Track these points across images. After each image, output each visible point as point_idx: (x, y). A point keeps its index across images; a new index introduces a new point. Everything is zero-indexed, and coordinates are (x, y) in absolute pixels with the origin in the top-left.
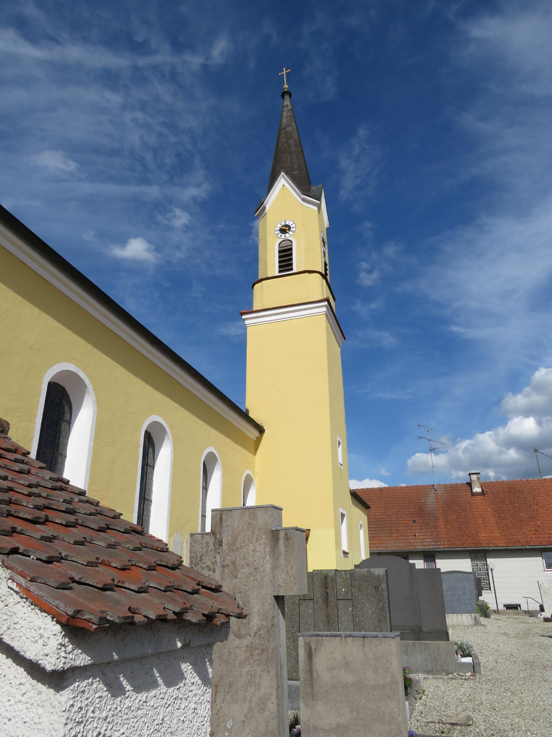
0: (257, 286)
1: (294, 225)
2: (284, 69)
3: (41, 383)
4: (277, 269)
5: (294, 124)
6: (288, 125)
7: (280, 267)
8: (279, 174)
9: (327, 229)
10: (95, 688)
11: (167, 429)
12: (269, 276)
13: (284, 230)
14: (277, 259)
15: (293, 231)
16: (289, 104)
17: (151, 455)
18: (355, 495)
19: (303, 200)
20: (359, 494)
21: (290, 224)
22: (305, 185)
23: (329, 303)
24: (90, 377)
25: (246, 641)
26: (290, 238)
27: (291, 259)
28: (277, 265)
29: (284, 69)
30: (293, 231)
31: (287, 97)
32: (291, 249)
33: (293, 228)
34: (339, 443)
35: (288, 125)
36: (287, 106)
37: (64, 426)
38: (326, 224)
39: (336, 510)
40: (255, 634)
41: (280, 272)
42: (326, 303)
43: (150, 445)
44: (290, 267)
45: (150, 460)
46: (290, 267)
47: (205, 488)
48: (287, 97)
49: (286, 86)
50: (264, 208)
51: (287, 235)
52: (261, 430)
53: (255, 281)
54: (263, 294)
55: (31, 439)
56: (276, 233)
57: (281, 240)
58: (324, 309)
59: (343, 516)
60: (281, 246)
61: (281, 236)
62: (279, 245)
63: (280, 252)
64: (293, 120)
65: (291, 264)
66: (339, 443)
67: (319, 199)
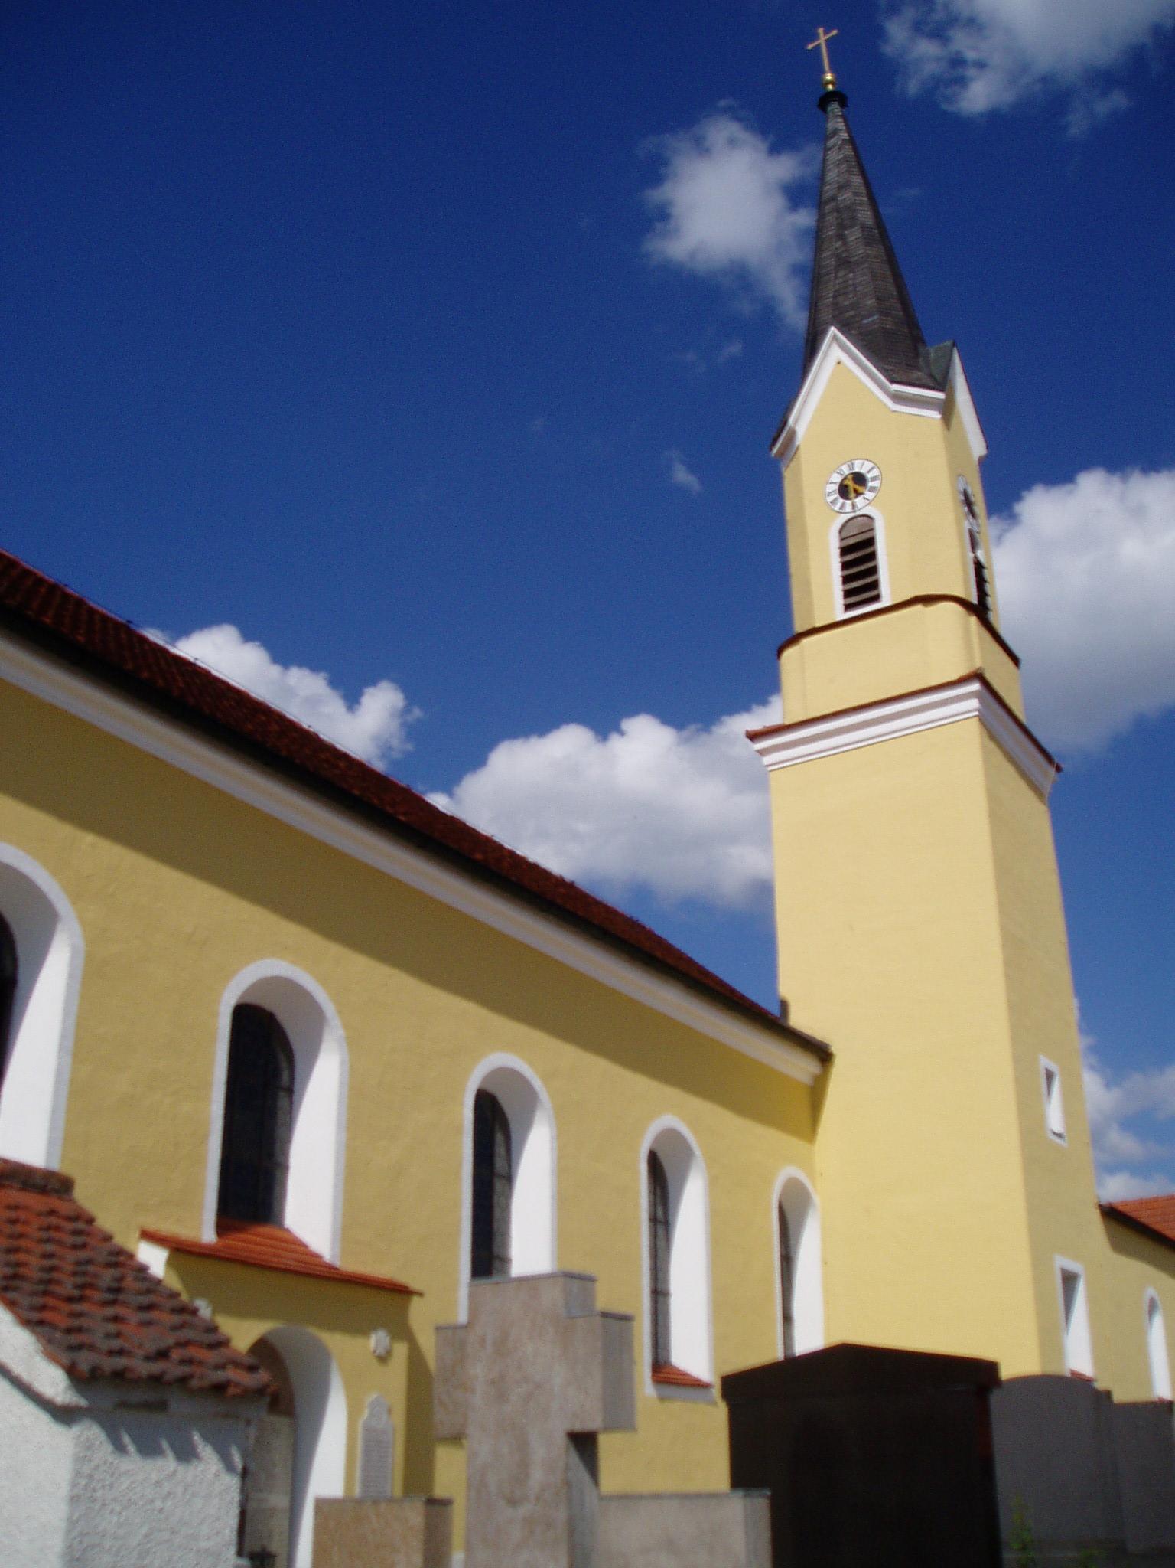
0: (789, 654)
1: (875, 472)
2: (821, 31)
3: (216, 1015)
4: (839, 600)
5: (857, 180)
6: (841, 188)
7: (848, 594)
8: (824, 332)
9: (983, 462)
10: (91, 1431)
11: (537, 1083)
12: (818, 624)
13: (853, 485)
14: (836, 573)
15: (872, 489)
16: (841, 125)
17: (500, 1150)
18: (1112, 1214)
19: (897, 398)
20: (1133, 1214)
21: (863, 471)
22: (902, 351)
23: (986, 684)
24: (323, 981)
25: (524, 1510)
26: (868, 511)
27: (874, 570)
28: (838, 588)
29: (821, 31)
30: (872, 489)
31: (834, 107)
32: (871, 542)
33: (874, 479)
34: (1050, 1076)
35: (841, 188)
36: (835, 132)
37: (283, 1101)
38: (977, 446)
39: (1039, 1261)
40: (538, 1499)
41: (848, 607)
42: (976, 686)
43: (494, 1127)
44: (873, 593)
45: (499, 1163)
46: (873, 593)
47: (661, 1222)
48: (834, 107)
49: (829, 77)
50: (792, 434)
51: (859, 501)
52: (822, 1054)
53: (784, 639)
54: (810, 675)
55: (205, 1137)
56: (830, 499)
57: (844, 518)
58: (974, 703)
59: (1069, 1280)
60: (844, 535)
61: (843, 506)
62: (840, 532)
63: (845, 551)
64: (855, 170)
65: (875, 585)
66: (1050, 1076)
67: (942, 383)
